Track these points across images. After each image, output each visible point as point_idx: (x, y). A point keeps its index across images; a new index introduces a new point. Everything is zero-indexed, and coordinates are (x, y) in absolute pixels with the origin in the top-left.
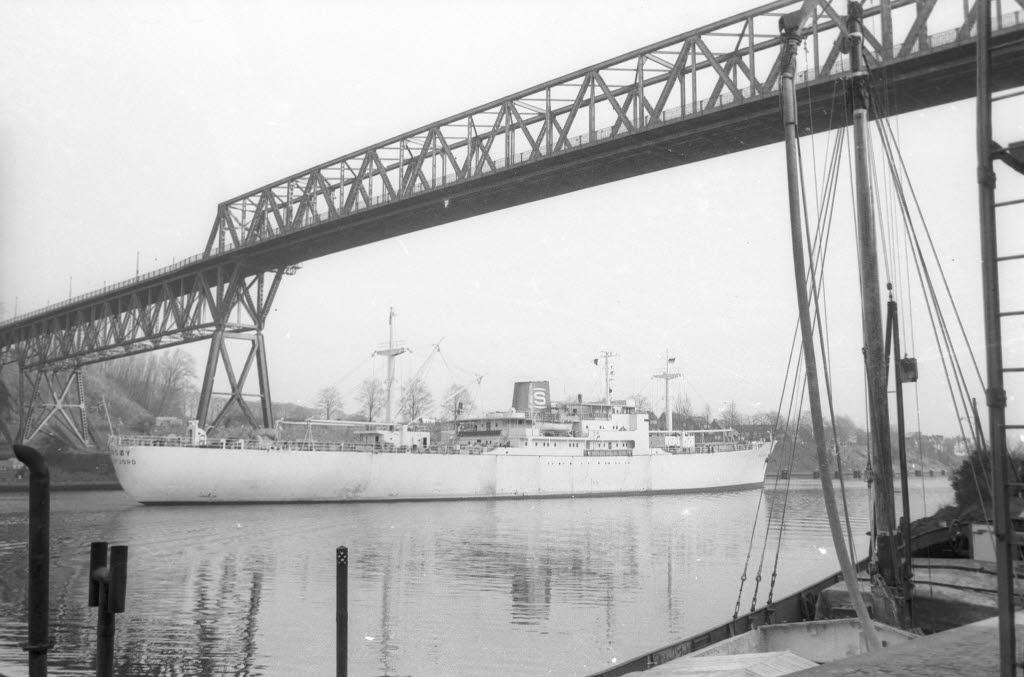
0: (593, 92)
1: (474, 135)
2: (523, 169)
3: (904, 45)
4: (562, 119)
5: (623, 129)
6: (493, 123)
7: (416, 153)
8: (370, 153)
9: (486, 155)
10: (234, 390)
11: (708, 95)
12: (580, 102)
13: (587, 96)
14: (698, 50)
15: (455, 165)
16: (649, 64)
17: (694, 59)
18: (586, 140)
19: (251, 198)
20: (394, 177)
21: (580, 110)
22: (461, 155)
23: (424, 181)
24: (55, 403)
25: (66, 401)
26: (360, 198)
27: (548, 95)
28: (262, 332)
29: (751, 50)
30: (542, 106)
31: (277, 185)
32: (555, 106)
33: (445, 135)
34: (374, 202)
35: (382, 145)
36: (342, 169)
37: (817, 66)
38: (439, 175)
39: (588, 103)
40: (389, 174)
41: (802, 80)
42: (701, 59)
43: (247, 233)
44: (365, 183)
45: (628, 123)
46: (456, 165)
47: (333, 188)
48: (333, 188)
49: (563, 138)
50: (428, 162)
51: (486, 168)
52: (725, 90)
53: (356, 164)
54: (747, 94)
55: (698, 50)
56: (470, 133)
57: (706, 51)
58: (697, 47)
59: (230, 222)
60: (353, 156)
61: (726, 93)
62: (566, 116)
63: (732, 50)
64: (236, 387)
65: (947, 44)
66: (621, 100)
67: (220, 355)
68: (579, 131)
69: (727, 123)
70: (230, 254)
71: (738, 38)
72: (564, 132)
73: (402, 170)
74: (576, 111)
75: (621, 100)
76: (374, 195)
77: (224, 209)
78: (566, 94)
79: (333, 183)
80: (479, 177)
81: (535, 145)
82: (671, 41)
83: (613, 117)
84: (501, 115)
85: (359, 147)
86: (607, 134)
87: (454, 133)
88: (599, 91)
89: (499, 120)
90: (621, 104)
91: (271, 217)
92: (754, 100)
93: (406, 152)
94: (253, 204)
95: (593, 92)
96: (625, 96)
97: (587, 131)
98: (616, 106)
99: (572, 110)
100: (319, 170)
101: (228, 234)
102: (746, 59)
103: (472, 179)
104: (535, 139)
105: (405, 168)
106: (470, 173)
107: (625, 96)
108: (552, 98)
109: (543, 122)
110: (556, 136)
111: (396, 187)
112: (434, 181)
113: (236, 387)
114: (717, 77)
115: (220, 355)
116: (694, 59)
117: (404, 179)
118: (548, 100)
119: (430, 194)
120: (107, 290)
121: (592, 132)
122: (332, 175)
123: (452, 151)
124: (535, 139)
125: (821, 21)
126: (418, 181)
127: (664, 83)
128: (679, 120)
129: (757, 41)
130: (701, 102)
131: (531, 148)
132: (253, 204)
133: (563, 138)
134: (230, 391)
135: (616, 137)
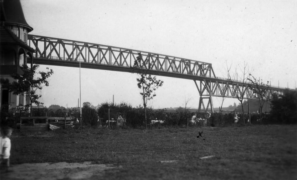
23: (163, 69)
28: (200, 96)
85: (148, 51)
104: (116, 58)
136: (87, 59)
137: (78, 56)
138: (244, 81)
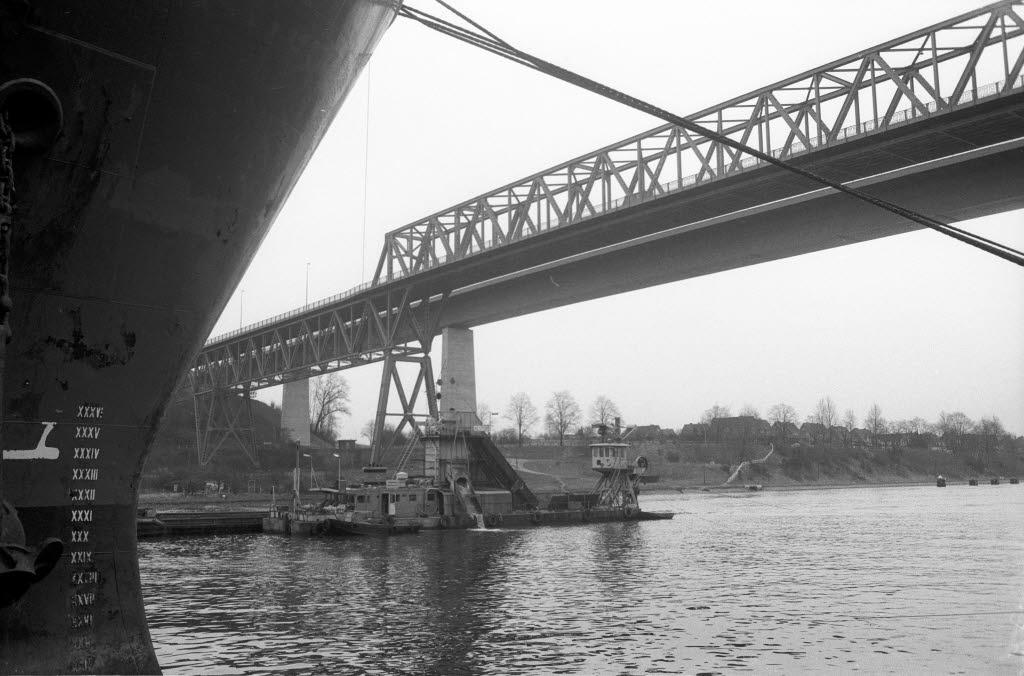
0: (679, 141)
1: (573, 181)
2: (551, 234)
3: (885, 117)
4: (653, 165)
5: (707, 176)
6: (663, 146)
7: (522, 199)
8: (537, 180)
9: (586, 201)
10: (405, 412)
11: (782, 145)
12: (668, 151)
13: (674, 144)
14: (876, 66)
15: (557, 210)
16: (824, 82)
17: (767, 110)
18: (674, 186)
19: (418, 228)
20: (503, 221)
21: (668, 157)
22: (562, 200)
23: (531, 226)
24: (227, 425)
25: (235, 427)
26: (474, 242)
27: (720, 116)
28: (429, 355)
29: (872, 82)
30: (634, 156)
31: (443, 214)
32: (645, 154)
33: (613, 159)
34: (487, 246)
35: (615, 147)
36: (510, 196)
37: (876, 119)
38: (544, 219)
39: (674, 150)
40: (556, 197)
41: (903, 118)
42: (772, 110)
43: (414, 261)
44: (478, 226)
45: (711, 172)
46: (559, 210)
47: (448, 232)
48: (448, 232)
49: (655, 184)
50: (534, 206)
51: (586, 213)
52: (796, 140)
53: (524, 191)
54: (814, 143)
55: (770, 103)
56: (570, 180)
57: (776, 103)
58: (875, 63)
59: (398, 251)
60: (520, 183)
61: (905, 103)
62: (657, 162)
63: (909, 63)
64: (408, 408)
65: (989, 97)
66: (794, 116)
67: (392, 379)
68: (668, 178)
69: (983, 117)
70: (400, 282)
71: (807, 91)
72: (655, 177)
73: (510, 216)
74: (665, 157)
75: (794, 116)
76: (486, 239)
77: (391, 239)
78: (744, 113)
79: (448, 227)
80: (579, 221)
81: (629, 190)
82: (914, 35)
83: (697, 166)
84: (671, 138)
86: (693, 181)
87: (448, 221)
88: (683, 141)
89: (669, 143)
90: (794, 119)
91: (438, 243)
92: (940, 114)
93: (513, 199)
94: (465, 216)
95: (679, 141)
96: (797, 113)
97: (676, 178)
98: (789, 120)
99: (662, 156)
100: (606, 153)
101: (396, 262)
102: (927, 73)
103: (824, 148)
105: (513, 212)
106: (571, 219)
107: (797, 113)
108: (938, 46)
109: (635, 168)
110: (648, 181)
111: (505, 230)
112: (539, 226)
113: (408, 408)
114: (789, 130)
115: (392, 379)
116: (767, 110)
117: (512, 224)
118: (640, 150)
119: (665, 198)
120: (244, 330)
121: (680, 179)
122: (448, 221)
123: (621, 173)
124: (628, 185)
125: (878, 74)
126: (526, 225)
127: (658, 160)
128: (971, 105)
129: (939, 53)
130: (865, 124)
131: (624, 195)
132: (465, 216)
133: (655, 184)
134: (402, 412)
135: (700, 184)
136: (544, 219)
137: (580, 208)
138: (680, 179)
